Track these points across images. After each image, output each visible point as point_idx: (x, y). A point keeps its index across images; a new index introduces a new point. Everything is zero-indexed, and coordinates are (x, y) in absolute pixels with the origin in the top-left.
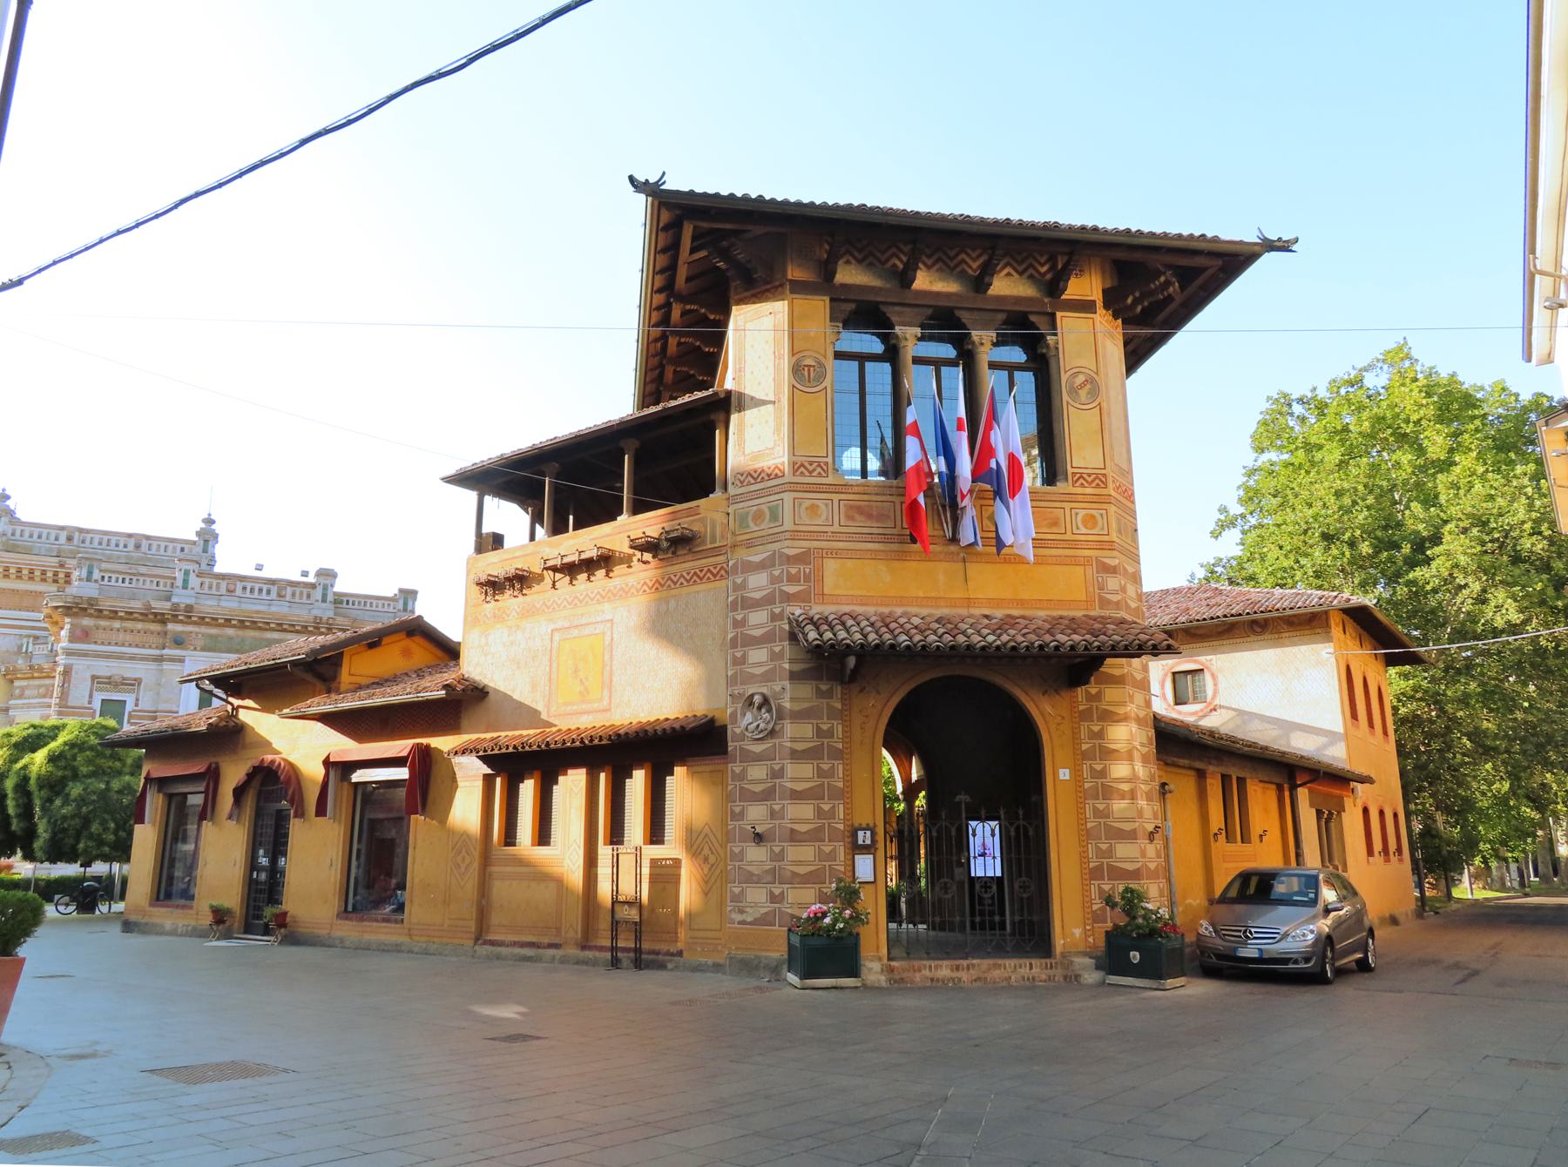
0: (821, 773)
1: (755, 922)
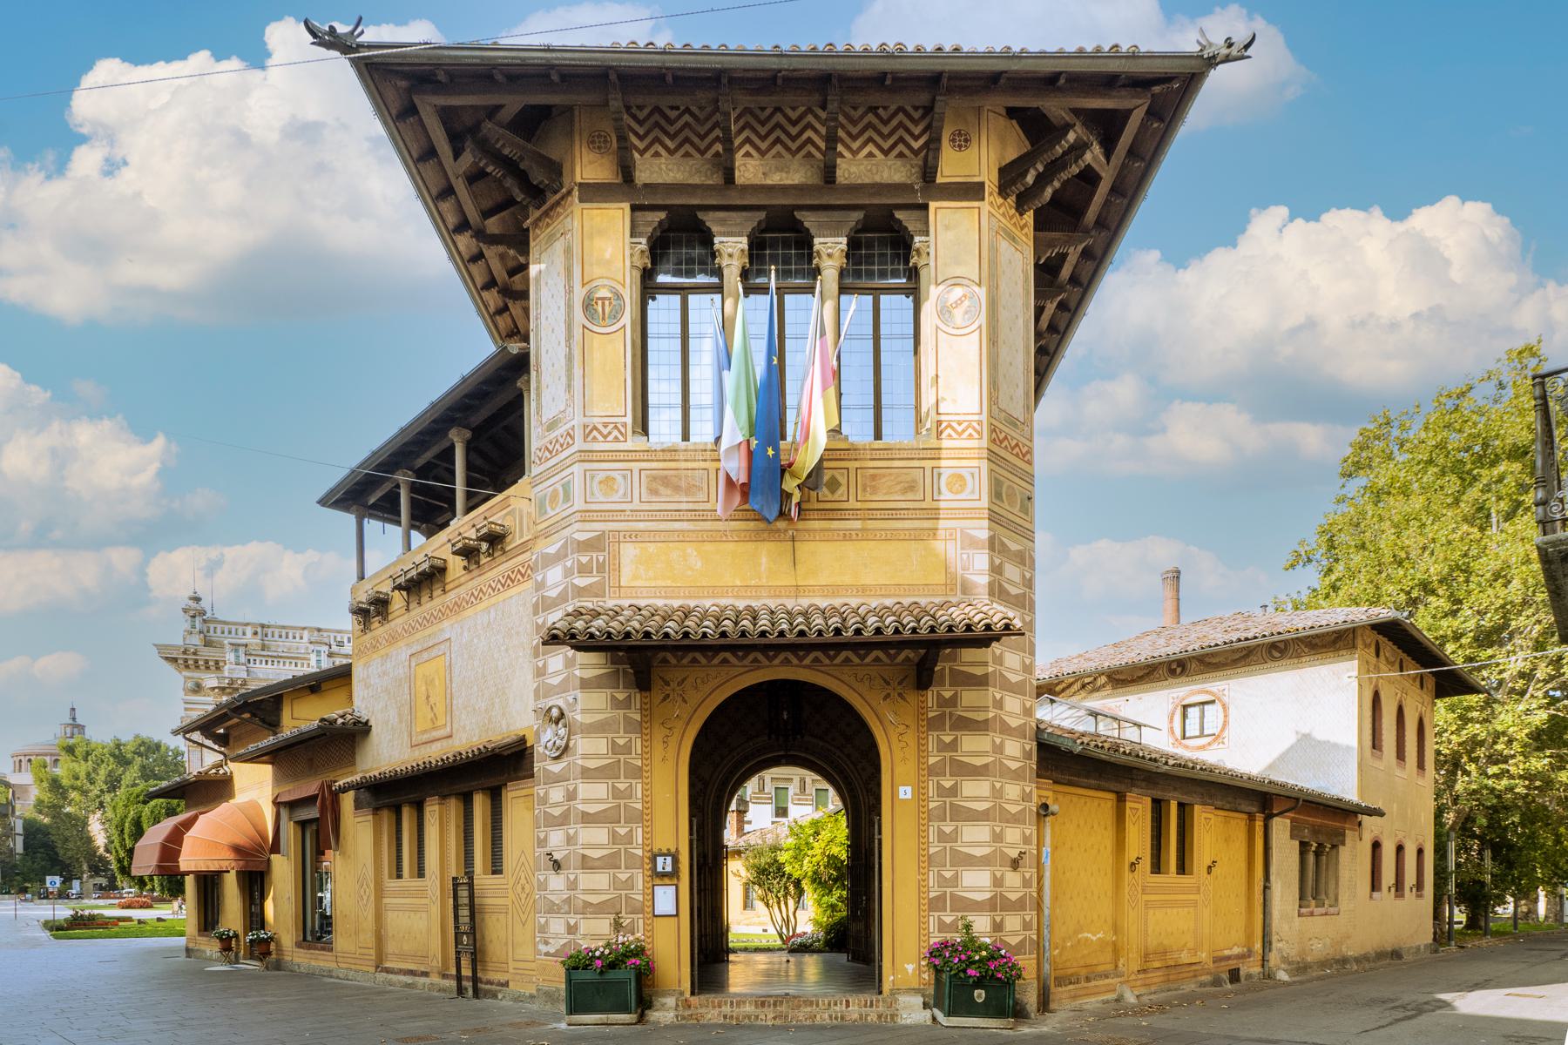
0: (616, 794)
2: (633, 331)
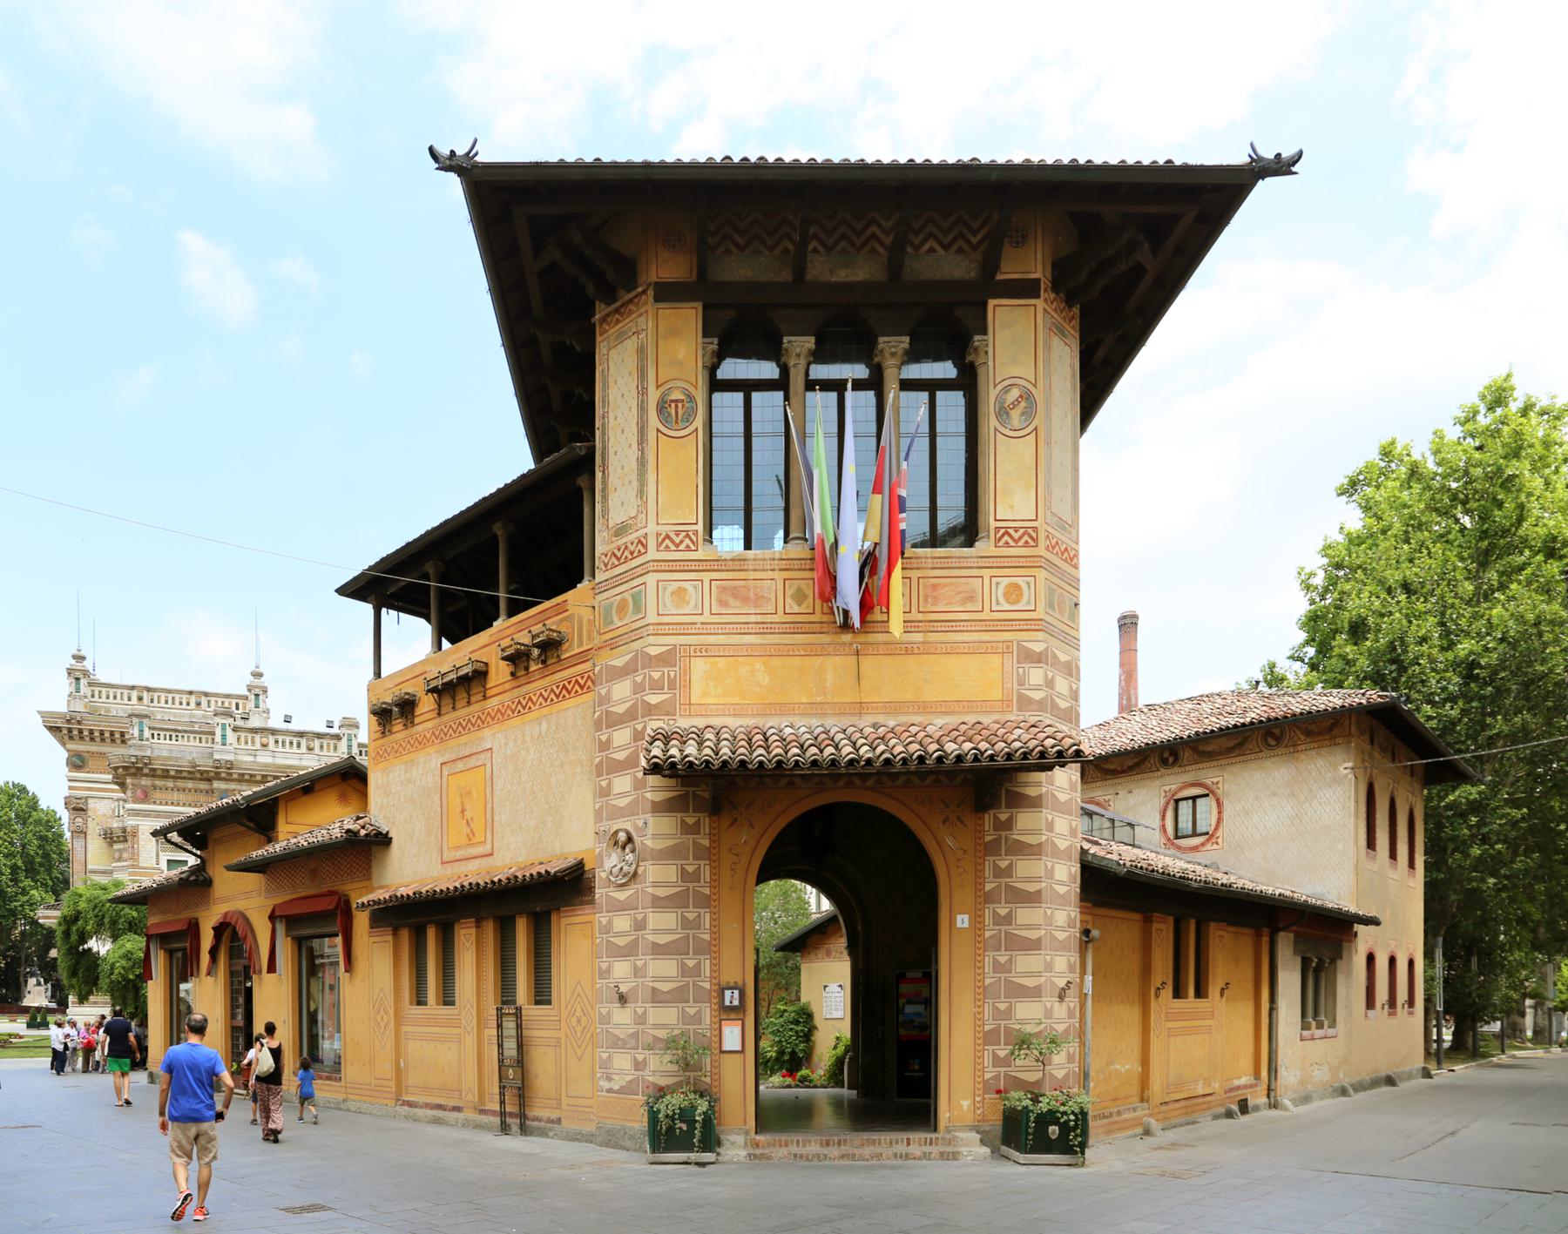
1: (622, 1091)
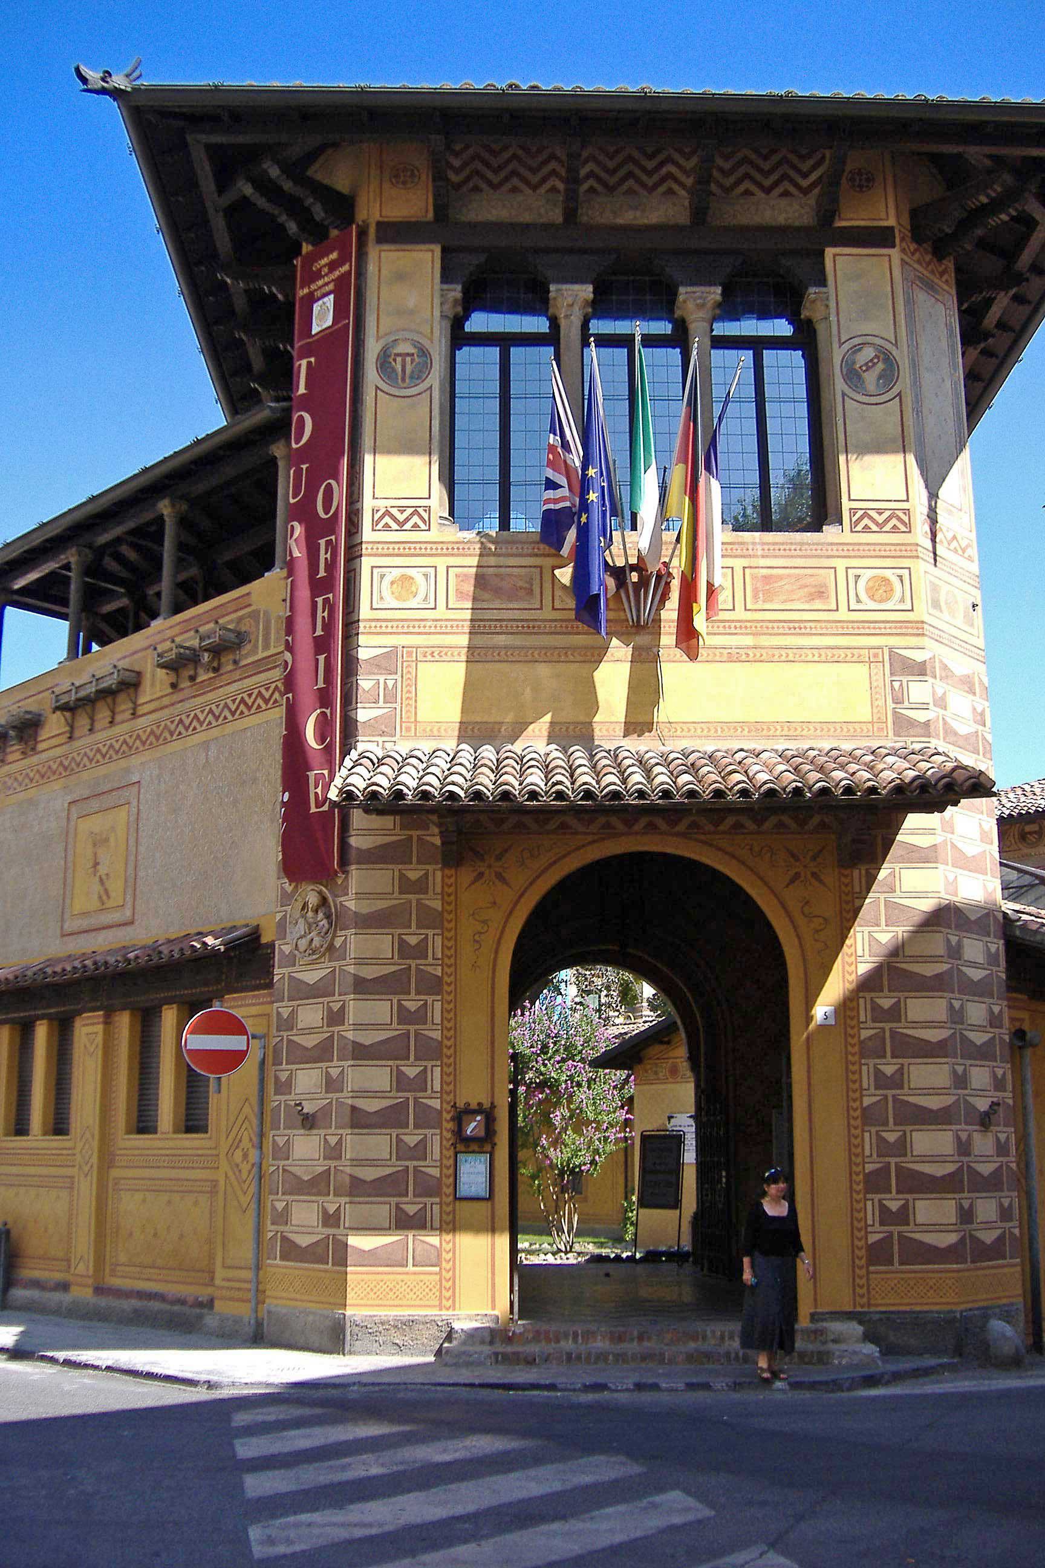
2: (442, 391)
